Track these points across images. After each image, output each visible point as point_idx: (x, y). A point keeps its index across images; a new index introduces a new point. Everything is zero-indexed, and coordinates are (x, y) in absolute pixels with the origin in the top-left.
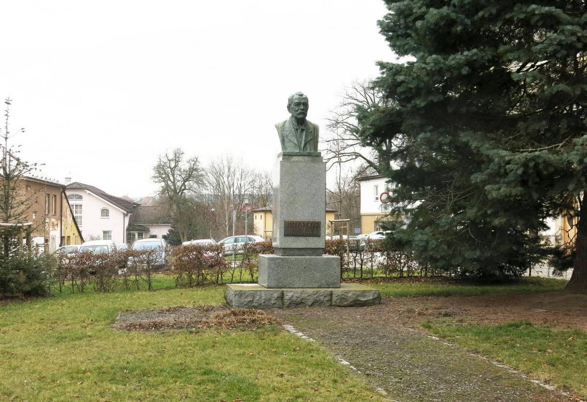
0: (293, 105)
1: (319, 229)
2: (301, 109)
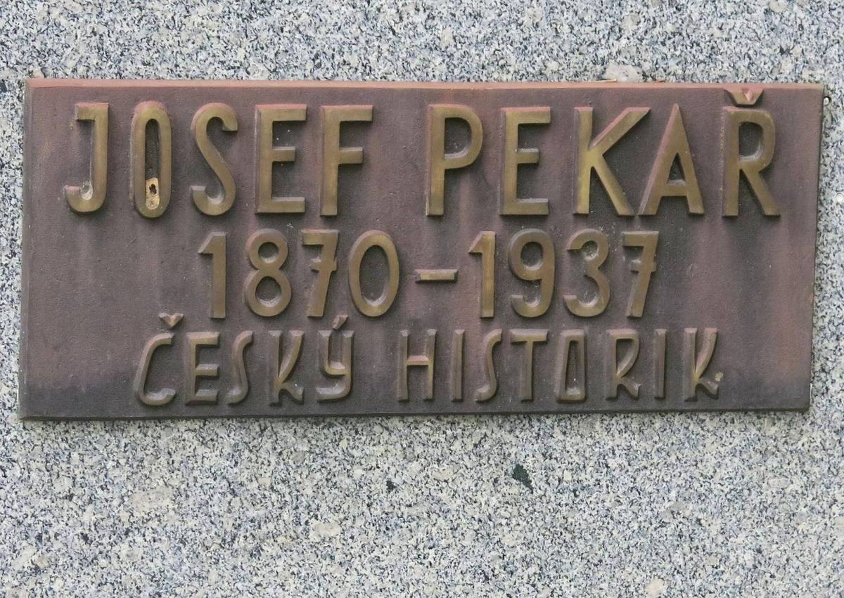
1: (778, 246)
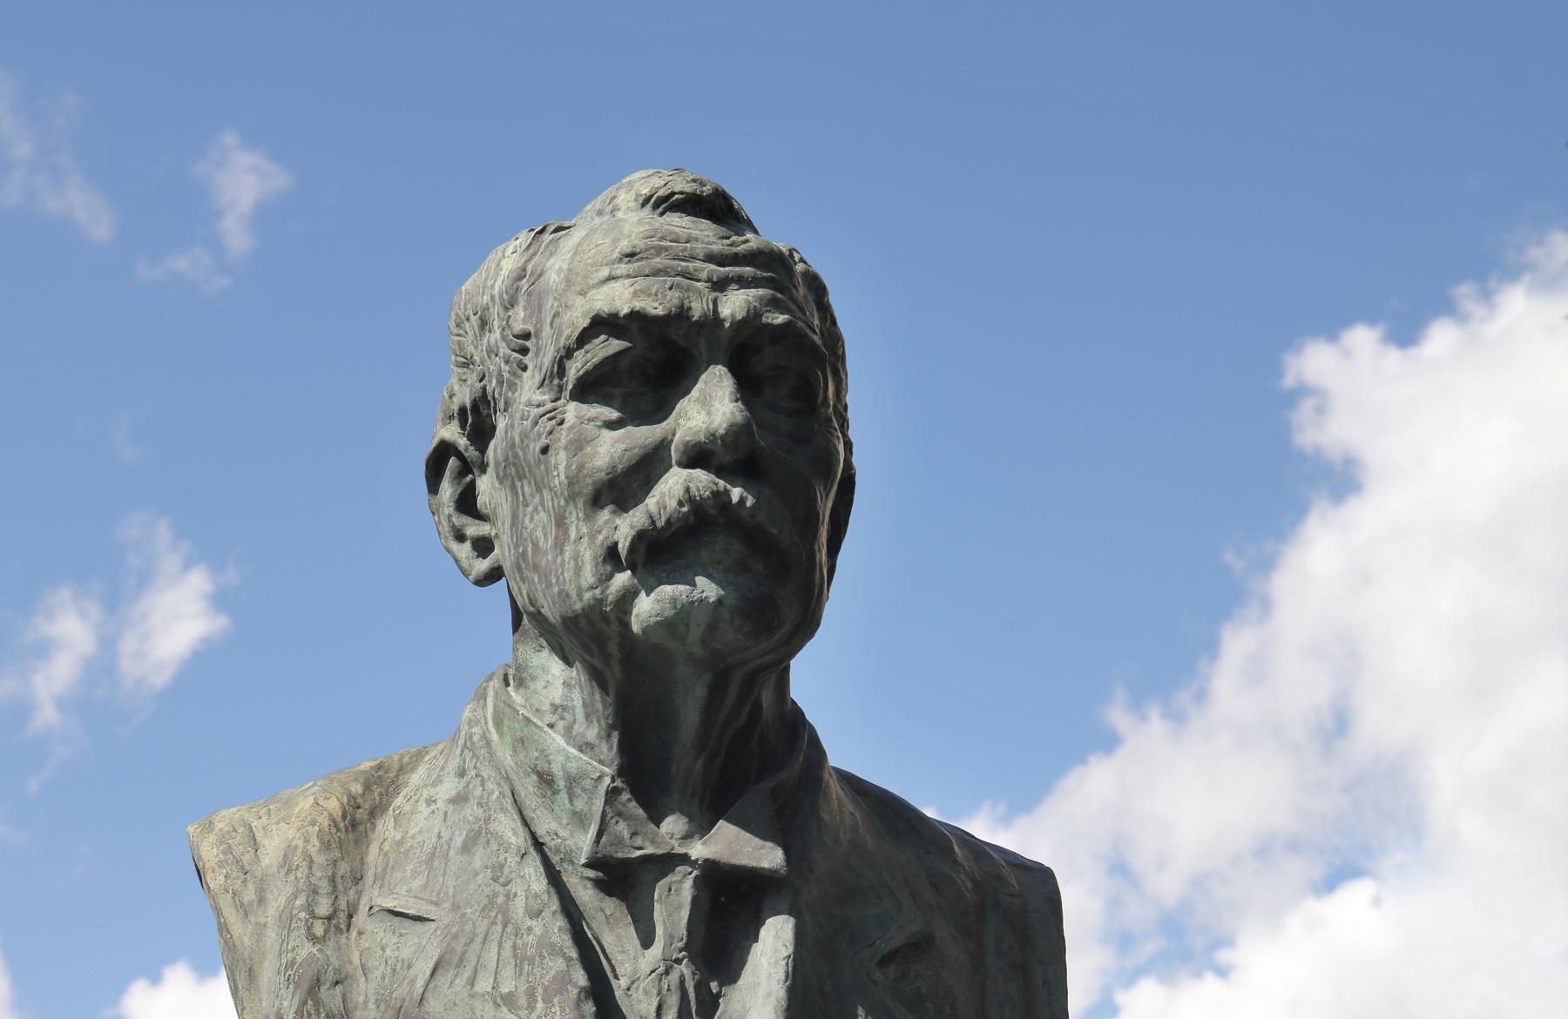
0: (529, 392)
2: (697, 456)
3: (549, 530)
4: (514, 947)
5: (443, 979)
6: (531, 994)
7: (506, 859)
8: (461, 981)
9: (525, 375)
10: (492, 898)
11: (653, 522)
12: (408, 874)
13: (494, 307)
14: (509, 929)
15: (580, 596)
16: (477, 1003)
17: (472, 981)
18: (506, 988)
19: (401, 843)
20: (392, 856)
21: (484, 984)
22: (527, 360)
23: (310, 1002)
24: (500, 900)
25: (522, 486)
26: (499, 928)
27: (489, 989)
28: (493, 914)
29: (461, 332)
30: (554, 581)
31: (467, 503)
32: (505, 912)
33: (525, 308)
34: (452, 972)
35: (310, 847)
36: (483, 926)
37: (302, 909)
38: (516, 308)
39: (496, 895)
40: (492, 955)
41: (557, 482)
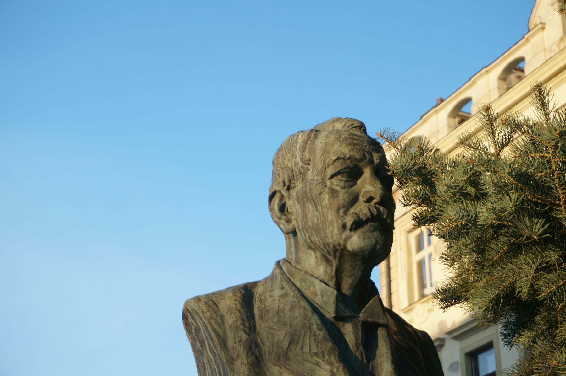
3: (319, 217)
4: (315, 339)
5: (293, 348)
6: (323, 353)
7: (307, 314)
8: (298, 349)
9: (309, 172)
10: (304, 325)
11: (358, 217)
12: (271, 317)
13: (297, 151)
14: (312, 334)
15: (332, 238)
16: (305, 355)
17: (302, 348)
18: (314, 350)
19: (264, 308)
20: (263, 312)
21: (306, 349)
22: (310, 167)
23: (250, 352)
24: (307, 325)
25: (308, 205)
26: (308, 334)
27: (308, 351)
28: (306, 329)
29: (283, 158)
30: (322, 232)
31: (283, 208)
32: (310, 328)
33: (308, 153)
34: (295, 346)
35: (238, 307)
36: (303, 333)
37: (240, 325)
38: (305, 152)
39: (306, 324)
40: (307, 341)
41: (324, 204)
